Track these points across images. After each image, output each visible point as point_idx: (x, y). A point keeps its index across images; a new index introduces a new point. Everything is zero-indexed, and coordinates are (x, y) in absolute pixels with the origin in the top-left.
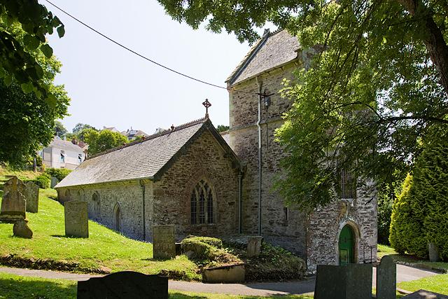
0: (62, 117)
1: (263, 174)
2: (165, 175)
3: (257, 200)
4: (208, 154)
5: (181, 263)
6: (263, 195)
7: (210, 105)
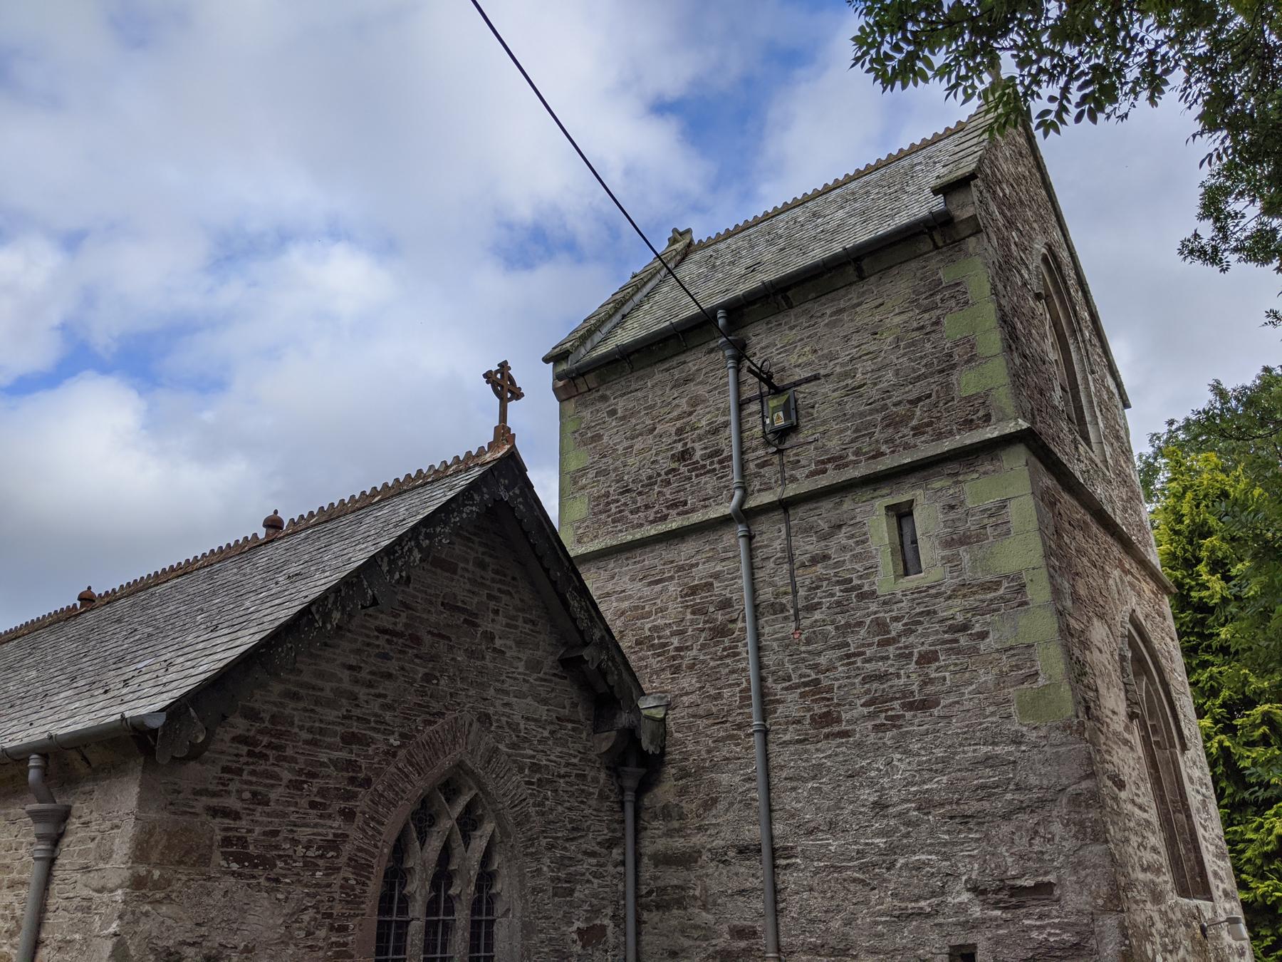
0: (1201, 117)
1: (781, 756)
2: (240, 725)
3: (750, 912)
4: (490, 637)
5: (1154, 931)
6: (789, 880)
7: (517, 395)
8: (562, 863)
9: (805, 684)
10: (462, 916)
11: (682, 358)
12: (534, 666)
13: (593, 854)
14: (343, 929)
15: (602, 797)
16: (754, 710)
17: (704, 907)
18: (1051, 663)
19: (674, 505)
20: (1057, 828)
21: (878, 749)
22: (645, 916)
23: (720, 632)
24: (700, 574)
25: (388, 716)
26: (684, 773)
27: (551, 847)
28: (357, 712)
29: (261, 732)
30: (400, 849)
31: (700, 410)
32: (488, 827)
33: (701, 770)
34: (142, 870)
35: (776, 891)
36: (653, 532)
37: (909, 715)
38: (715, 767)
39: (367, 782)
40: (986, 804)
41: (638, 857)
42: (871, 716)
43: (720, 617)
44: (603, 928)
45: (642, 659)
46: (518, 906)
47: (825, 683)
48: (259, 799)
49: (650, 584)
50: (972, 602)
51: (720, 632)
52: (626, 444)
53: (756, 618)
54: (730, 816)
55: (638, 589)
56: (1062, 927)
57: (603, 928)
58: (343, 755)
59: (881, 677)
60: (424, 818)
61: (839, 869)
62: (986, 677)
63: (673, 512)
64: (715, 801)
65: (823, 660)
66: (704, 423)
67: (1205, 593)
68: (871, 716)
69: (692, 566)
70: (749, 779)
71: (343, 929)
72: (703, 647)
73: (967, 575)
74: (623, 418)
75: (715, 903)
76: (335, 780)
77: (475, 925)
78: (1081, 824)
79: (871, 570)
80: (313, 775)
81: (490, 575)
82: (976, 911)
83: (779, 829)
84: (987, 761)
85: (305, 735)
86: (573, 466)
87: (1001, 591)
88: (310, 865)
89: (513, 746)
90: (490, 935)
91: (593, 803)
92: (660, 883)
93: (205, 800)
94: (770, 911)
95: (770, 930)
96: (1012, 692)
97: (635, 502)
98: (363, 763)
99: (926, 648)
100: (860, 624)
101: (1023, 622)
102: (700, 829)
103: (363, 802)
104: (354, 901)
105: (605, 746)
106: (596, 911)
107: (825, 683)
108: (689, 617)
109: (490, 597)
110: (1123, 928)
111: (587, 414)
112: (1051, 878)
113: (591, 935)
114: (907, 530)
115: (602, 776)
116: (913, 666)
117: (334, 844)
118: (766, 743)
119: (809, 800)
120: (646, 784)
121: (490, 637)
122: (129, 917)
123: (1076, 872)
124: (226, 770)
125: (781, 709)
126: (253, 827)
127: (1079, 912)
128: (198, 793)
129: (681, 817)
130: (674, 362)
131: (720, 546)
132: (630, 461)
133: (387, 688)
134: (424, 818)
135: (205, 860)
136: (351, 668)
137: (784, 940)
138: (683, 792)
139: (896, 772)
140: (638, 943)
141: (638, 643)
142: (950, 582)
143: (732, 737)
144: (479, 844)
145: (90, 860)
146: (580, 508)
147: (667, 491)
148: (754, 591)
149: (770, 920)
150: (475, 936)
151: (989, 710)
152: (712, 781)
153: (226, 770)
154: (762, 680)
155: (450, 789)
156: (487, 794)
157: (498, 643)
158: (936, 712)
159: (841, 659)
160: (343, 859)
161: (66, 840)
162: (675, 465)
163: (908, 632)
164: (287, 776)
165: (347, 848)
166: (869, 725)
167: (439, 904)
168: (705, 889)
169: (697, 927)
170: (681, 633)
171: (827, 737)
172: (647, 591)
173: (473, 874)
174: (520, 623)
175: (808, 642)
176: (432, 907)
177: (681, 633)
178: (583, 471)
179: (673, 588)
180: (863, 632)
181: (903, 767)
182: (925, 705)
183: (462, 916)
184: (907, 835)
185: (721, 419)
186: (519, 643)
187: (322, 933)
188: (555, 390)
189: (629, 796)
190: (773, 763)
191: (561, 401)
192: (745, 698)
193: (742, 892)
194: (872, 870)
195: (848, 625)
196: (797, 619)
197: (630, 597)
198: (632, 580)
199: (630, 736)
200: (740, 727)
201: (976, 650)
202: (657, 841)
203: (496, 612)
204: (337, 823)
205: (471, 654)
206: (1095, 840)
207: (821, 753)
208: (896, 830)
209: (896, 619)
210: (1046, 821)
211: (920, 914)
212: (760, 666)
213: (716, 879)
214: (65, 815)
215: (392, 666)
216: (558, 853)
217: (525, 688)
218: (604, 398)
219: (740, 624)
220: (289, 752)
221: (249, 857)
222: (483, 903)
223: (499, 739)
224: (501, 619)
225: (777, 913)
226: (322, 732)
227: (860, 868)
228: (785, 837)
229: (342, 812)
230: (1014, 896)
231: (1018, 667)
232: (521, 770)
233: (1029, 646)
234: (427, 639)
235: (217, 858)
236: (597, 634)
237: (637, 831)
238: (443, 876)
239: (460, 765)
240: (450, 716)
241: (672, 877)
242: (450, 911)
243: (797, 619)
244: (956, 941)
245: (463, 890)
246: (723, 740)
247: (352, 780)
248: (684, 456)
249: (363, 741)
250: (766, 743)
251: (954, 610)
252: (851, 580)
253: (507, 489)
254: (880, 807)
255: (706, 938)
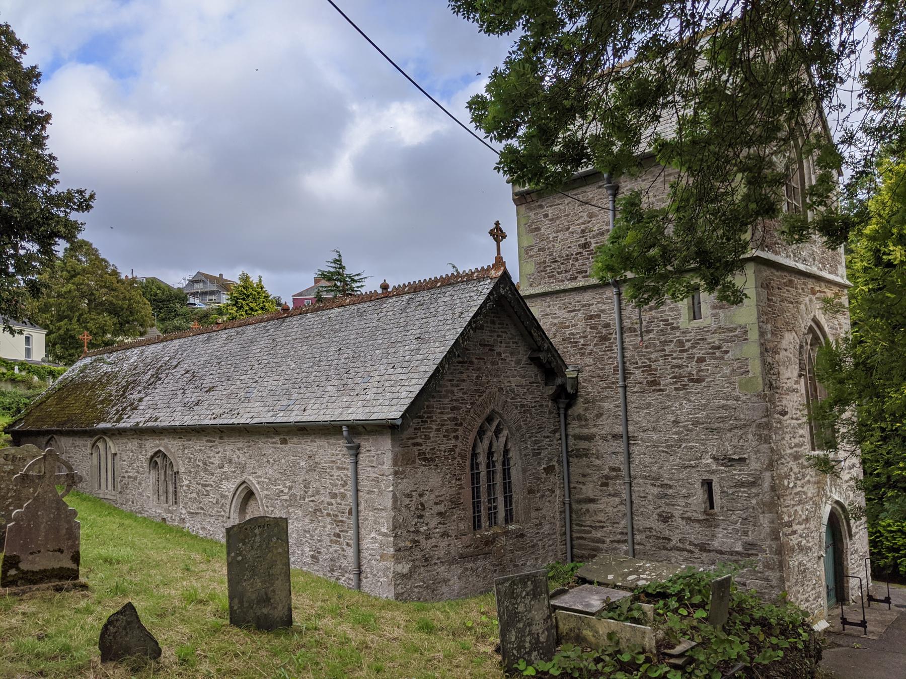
1: (632, 398)
3: (619, 461)
4: (499, 354)
6: (635, 450)
8: (535, 442)
9: (644, 367)
10: (499, 468)
11: (584, 189)
12: (518, 362)
13: (548, 437)
14: (460, 479)
15: (550, 413)
16: (620, 376)
17: (597, 458)
18: (755, 367)
19: (580, 272)
20: (750, 436)
21: (676, 398)
22: (571, 459)
23: (604, 338)
24: (594, 310)
25: (465, 397)
26: (587, 401)
27: (530, 437)
28: (454, 398)
29: (424, 413)
30: (474, 447)
31: (594, 220)
32: (505, 432)
33: (594, 401)
34: (396, 469)
35: (629, 454)
36: (570, 287)
37: (691, 384)
38: (601, 400)
39: (461, 424)
40: (722, 425)
41: (567, 436)
42: (674, 383)
43: (604, 331)
44: (554, 466)
45: (565, 348)
46: (520, 461)
47: (653, 367)
48: (427, 437)
49: (569, 312)
50: (722, 336)
51: (604, 338)
52: (554, 235)
53: (622, 334)
54: (608, 421)
55: (562, 314)
56: (748, 474)
57: (554, 466)
58: (452, 415)
59: (680, 367)
60: (481, 432)
61: (658, 447)
62: (726, 371)
63: (580, 276)
64: (602, 414)
65: (653, 356)
66: (596, 228)
67: (890, 257)
68: (674, 383)
69: (590, 305)
70: (617, 407)
71: (460, 479)
72: (595, 345)
73: (722, 324)
74: (552, 220)
75: (602, 457)
76: (450, 425)
77: (504, 470)
78: (760, 435)
79: (677, 317)
80: (443, 425)
81: (497, 326)
82: (714, 467)
83: (631, 428)
84: (723, 407)
85: (439, 411)
86: (525, 244)
87: (737, 333)
88: (447, 458)
89: (513, 398)
90: (509, 473)
91: (546, 416)
92: (577, 447)
93: (411, 441)
94: (626, 462)
95: (626, 469)
96: (737, 378)
97: (559, 268)
98: (459, 417)
99: (700, 355)
100: (671, 341)
101: (745, 348)
102: (595, 426)
103: (460, 432)
104: (462, 469)
105: (551, 392)
106: (550, 460)
107: (653, 367)
108: (589, 330)
109: (498, 336)
110: (773, 477)
111: (532, 214)
112: (746, 456)
113: (549, 470)
114: (696, 297)
115: (550, 404)
116: (694, 363)
117: (452, 450)
118: (625, 392)
119: (644, 417)
120: (569, 406)
121: (499, 354)
122: (395, 485)
123: (756, 454)
124: (415, 429)
125: (632, 377)
126: (426, 448)
127: (756, 470)
128: (408, 439)
129: (586, 420)
130: (580, 190)
131: (604, 296)
132: (557, 245)
133: (464, 385)
134: (481, 432)
135: (414, 462)
136: (450, 381)
137: (632, 473)
138: (587, 409)
139: (685, 409)
140: (568, 470)
141: (563, 340)
142: (714, 326)
143: (610, 387)
144: (502, 440)
145: (375, 464)
146: (531, 268)
147: (577, 264)
148: (621, 321)
149: (627, 466)
150: (504, 474)
151: (726, 385)
152: (600, 406)
153: (415, 429)
154: (624, 363)
155: (490, 419)
156: (504, 420)
157: (503, 356)
158: (703, 384)
159: (661, 356)
160: (457, 454)
161: (361, 455)
162: (581, 250)
163: (693, 347)
164: (434, 427)
165: (457, 450)
166: (673, 387)
167: (490, 464)
168: (598, 451)
169: (594, 466)
170: (585, 337)
171: (654, 391)
172: (567, 315)
173: (502, 452)
174: (511, 344)
175: (647, 347)
176: (488, 466)
177: (585, 337)
178: (530, 248)
179: (580, 315)
180: (672, 345)
181: (687, 407)
182: (699, 380)
183: (499, 468)
184: (687, 435)
185: (605, 228)
186: (512, 354)
187: (453, 482)
188: (514, 200)
189: (562, 411)
190: (628, 400)
191: (517, 205)
192: (616, 370)
193: (613, 453)
194: (671, 449)
195: (665, 341)
196: (642, 336)
197: (559, 317)
198: (560, 309)
199: (562, 388)
200: (613, 383)
201: (723, 358)
202: (575, 428)
203: (501, 342)
204: (453, 441)
205: (493, 363)
206: (765, 442)
207: (650, 398)
208: (682, 432)
209: (688, 341)
210: (746, 433)
211: (691, 466)
212: (623, 357)
213: (604, 447)
214: (359, 447)
215: (464, 376)
216: (534, 439)
217: (516, 373)
218: (541, 207)
219: (614, 336)
220: (434, 418)
221: (427, 459)
222: (506, 462)
223: (507, 397)
224: (503, 345)
225: (629, 462)
226: (444, 408)
227: (667, 447)
228: (634, 432)
229: (454, 437)
230: (729, 461)
231: (741, 368)
232: (517, 408)
233: (747, 359)
234: (476, 361)
235: (418, 461)
236: (546, 346)
237: (566, 425)
238: (490, 454)
239: (493, 410)
240: (488, 391)
241: (583, 445)
242: (494, 466)
243: (642, 336)
244: (704, 477)
245: (498, 458)
246: (605, 388)
247: (456, 424)
248: (586, 245)
249: (458, 408)
250: (625, 392)
251: (715, 339)
252: (668, 320)
253: (504, 289)
254: (676, 422)
255: (598, 470)
